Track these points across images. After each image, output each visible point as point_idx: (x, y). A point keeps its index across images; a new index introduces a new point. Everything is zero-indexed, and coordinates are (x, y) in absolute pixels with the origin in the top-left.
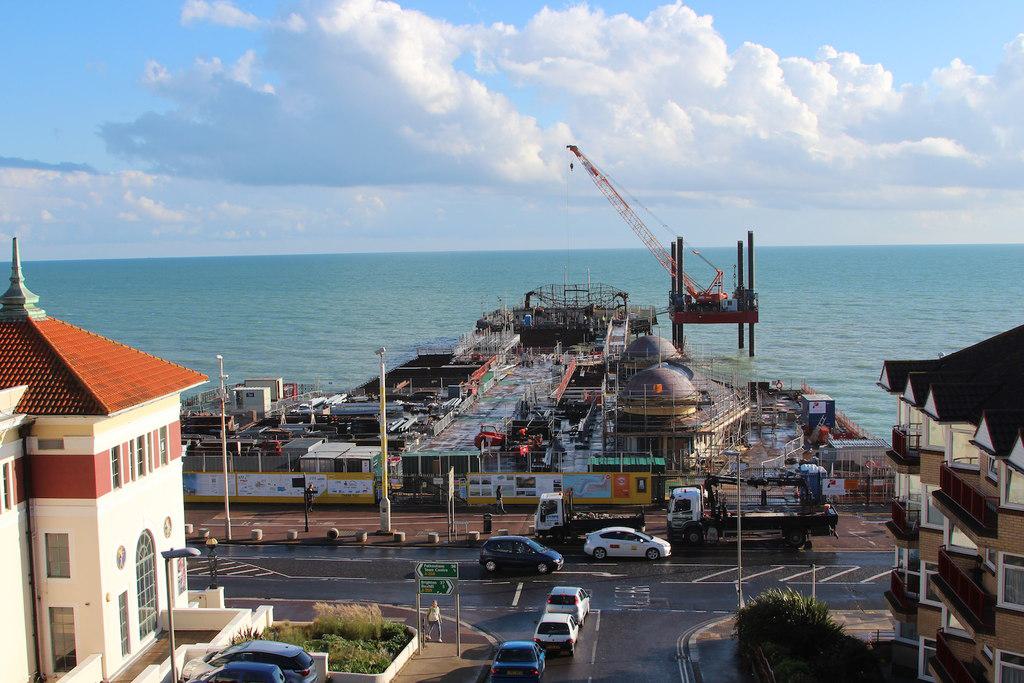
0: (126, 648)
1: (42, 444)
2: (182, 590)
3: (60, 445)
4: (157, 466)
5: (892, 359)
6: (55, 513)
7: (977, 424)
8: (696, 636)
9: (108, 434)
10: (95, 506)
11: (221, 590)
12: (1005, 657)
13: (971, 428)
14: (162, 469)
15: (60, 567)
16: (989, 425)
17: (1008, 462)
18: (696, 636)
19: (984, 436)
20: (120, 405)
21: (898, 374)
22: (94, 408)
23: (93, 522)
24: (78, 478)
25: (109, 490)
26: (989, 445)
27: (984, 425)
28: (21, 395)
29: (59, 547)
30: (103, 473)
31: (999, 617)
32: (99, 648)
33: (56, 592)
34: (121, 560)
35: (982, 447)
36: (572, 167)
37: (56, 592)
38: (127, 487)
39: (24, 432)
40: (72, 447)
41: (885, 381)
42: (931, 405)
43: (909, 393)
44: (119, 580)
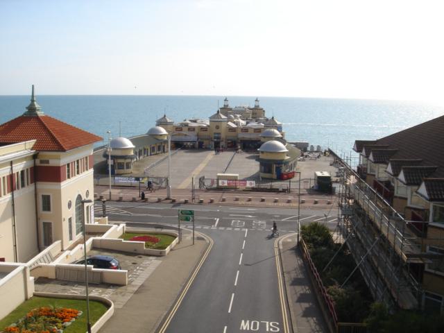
0: (71, 239)
1: (42, 162)
2: (77, 233)
3: (48, 162)
4: (84, 171)
5: (358, 140)
6: (46, 187)
7: (387, 164)
8: (282, 240)
9: (64, 160)
10: (60, 185)
11: (107, 217)
12: (427, 294)
13: (384, 166)
14: (86, 172)
15: (47, 207)
16: (426, 186)
17: (397, 179)
18: (282, 240)
19: (389, 169)
20: (71, 148)
21: (360, 146)
22: (61, 149)
23: (59, 192)
24: (55, 175)
25: (65, 180)
26: (391, 172)
27: (390, 166)
28: (33, 143)
29: (47, 199)
30: (64, 172)
31: (425, 275)
32: (60, 237)
33: (46, 217)
34: (70, 205)
35: (389, 173)
36: (133, 263)
37: (46, 217)
38: (73, 179)
39: (35, 157)
40: (53, 163)
41: (356, 148)
42: (371, 157)
43: (364, 153)
44: (68, 213)
